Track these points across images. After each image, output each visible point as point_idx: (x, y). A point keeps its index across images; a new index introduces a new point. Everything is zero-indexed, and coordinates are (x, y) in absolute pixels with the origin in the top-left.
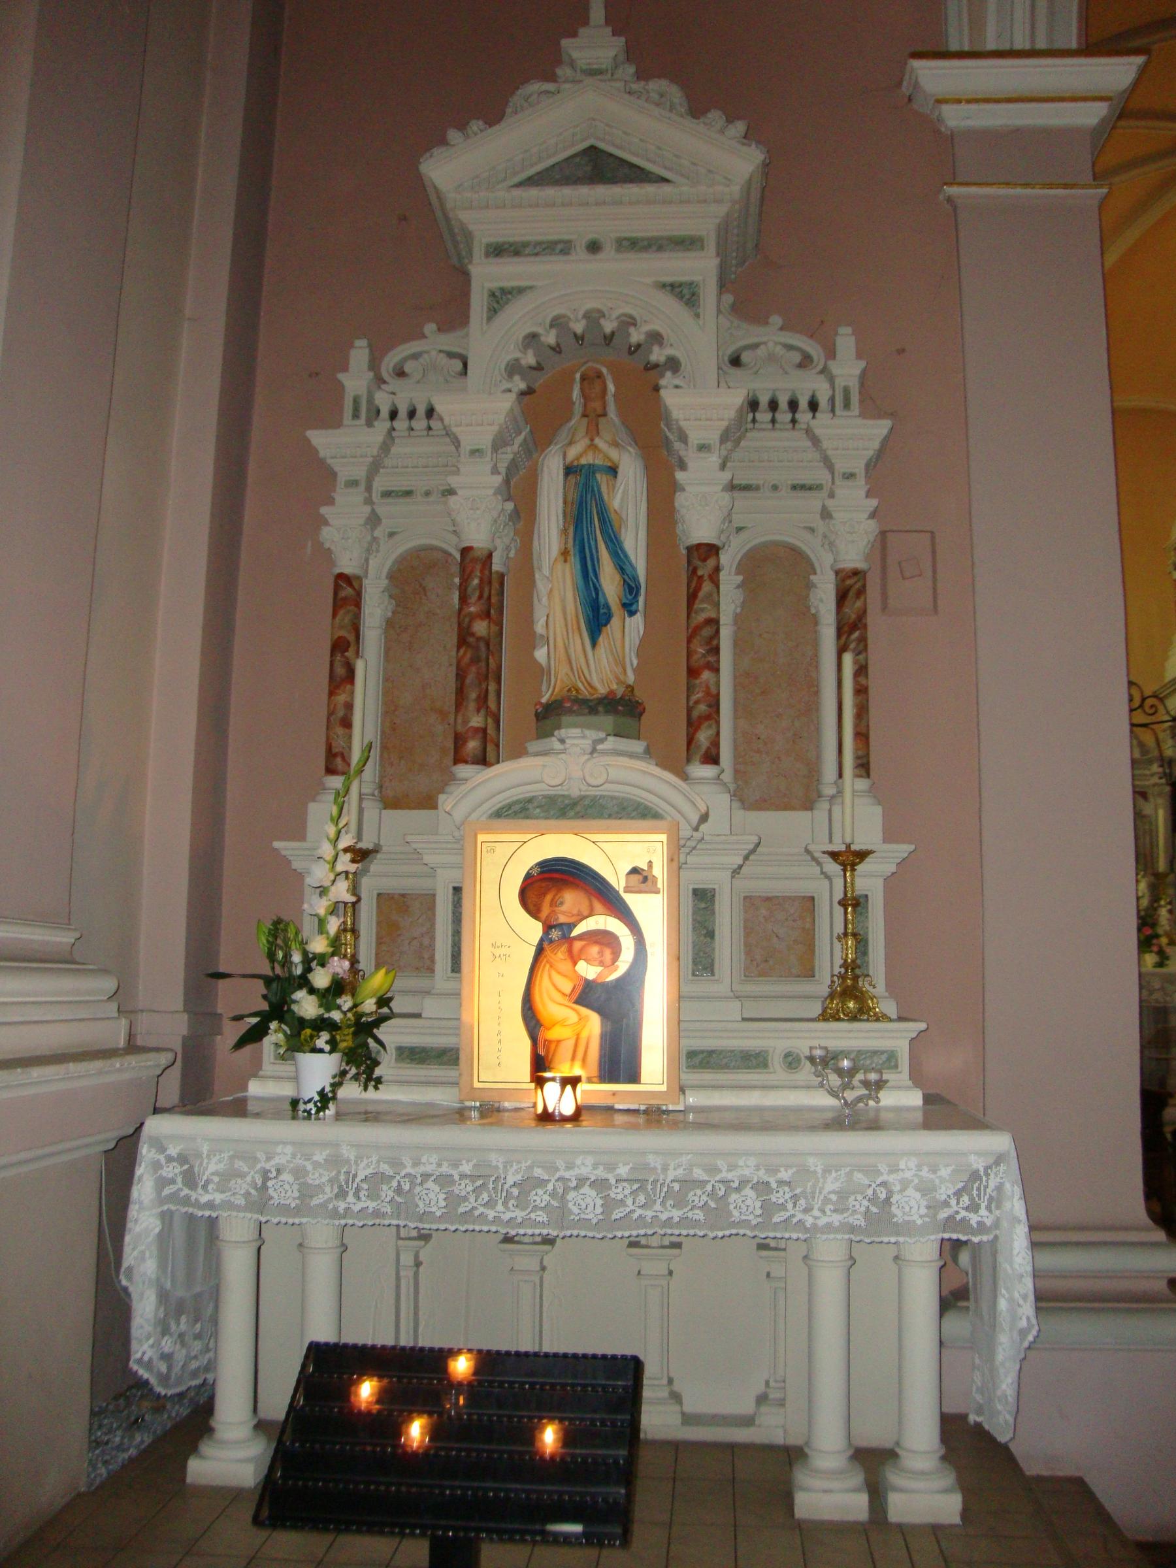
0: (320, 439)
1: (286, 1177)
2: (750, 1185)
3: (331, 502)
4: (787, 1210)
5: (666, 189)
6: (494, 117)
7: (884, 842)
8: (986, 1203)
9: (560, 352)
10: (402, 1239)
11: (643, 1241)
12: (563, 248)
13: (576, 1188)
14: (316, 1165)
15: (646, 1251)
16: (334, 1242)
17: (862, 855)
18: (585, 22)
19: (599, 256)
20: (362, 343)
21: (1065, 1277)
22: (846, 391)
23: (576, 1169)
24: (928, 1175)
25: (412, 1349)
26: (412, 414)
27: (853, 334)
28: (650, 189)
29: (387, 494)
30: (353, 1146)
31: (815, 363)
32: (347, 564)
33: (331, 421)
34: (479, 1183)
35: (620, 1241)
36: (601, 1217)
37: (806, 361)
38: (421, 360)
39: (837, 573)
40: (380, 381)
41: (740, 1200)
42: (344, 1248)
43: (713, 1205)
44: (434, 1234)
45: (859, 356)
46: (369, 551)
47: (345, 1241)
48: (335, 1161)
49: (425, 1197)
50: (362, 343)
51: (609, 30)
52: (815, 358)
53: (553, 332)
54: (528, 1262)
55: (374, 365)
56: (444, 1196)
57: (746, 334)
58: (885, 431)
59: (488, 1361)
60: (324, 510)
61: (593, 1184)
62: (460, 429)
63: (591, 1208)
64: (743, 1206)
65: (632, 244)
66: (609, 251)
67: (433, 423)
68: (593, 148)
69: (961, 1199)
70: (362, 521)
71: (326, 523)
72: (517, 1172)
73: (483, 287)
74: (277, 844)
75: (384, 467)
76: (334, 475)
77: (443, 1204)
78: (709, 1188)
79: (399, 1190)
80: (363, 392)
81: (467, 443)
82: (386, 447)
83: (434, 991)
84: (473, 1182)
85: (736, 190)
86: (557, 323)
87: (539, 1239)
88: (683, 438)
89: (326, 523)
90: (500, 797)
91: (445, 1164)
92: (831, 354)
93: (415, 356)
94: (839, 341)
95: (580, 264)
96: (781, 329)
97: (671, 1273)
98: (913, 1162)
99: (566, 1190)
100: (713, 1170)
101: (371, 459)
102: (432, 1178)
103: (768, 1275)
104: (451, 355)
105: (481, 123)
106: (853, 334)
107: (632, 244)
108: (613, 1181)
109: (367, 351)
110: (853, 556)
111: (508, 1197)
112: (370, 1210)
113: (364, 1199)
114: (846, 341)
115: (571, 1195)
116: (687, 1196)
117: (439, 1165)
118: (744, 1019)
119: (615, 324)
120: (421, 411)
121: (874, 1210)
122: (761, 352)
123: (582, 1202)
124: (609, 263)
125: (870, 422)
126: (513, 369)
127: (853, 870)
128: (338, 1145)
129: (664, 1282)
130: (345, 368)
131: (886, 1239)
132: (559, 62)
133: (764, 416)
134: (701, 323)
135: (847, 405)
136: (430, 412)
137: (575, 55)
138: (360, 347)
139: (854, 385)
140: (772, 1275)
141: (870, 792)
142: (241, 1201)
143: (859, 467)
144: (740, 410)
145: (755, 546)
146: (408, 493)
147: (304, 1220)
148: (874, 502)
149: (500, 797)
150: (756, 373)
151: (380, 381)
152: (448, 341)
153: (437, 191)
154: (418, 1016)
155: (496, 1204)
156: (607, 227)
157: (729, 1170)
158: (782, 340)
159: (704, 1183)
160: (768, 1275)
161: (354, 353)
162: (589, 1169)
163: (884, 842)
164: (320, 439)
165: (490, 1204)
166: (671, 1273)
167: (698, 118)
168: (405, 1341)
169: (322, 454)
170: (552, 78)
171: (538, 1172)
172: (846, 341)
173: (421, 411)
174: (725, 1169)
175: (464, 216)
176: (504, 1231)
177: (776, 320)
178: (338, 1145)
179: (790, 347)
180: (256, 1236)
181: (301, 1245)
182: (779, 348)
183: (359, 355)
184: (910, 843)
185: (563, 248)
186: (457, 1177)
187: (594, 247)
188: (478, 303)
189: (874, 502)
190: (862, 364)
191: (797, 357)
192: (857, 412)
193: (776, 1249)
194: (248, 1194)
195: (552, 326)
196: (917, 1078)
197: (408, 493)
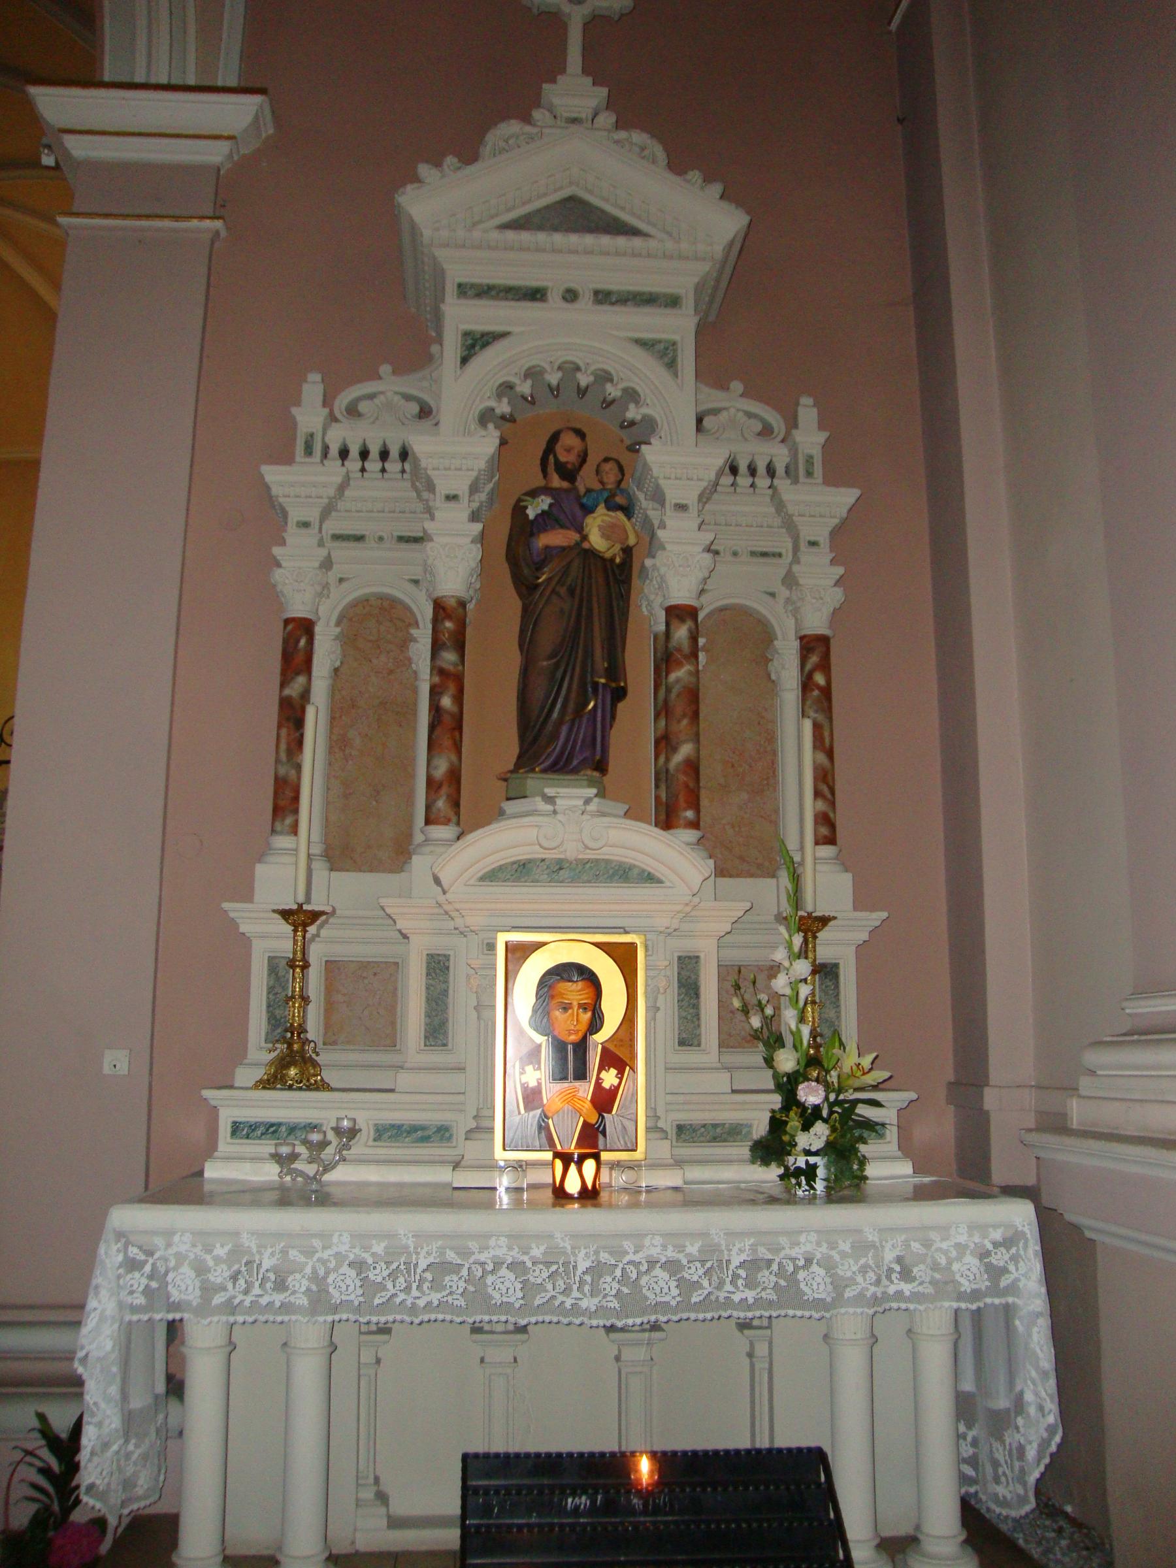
0: (273, 474)
1: (186, 1270)
2: (506, 1265)
3: (283, 543)
4: (546, 1291)
5: (637, 242)
6: (469, 156)
7: (855, 909)
8: (417, 1283)
9: (556, 397)
10: (365, 1333)
11: (487, 1327)
12: (536, 295)
13: (492, 1272)
14: (218, 1260)
15: (489, 1336)
16: (221, 1340)
17: (824, 921)
18: (563, 71)
19: (576, 305)
20: (314, 377)
21: (43, 1359)
22: (809, 460)
23: (490, 1250)
24: (674, 1254)
25: (770, 1451)
26: (364, 454)
27: (814, 405)
28: (621, 241)
29: (337, 537)
30: (253, 1234)
31: (775, 434)
32: (298, 609)
33: (285, 458)
34: (554, 1268)
35: (536, 1326)
36: (678, 1299)
37: (766, 432)
38: (376, 401)
39: (802, 638)
40: (333, 418)
41: (809, 1277)
42: (874, 1339)
43: (471, 1288)
44: (395, 1327)
45: (821, 427)
46: (320, 595)
47: (233, 1339)
48: (236, 1252)
49: (501, 1286)
50: (314, 377)
51: (589, 80)
52: (775, 425)
53: (529, 382)
54: (500, 1354)
55: (327, 401)
56: (675, 1283)
57: (713, 398)
58: (852, 500)
59: (664, 1460)
60: (277, 551)
61: (512, 1267)
62: (436, 472)
63: (511, 1291)
64: (656, 1287)
65: (603, 297)
66: (586, 301)
67: (407, 466)
68: (572, 199)
69: (1019, 1265)
70: (317, 564)
71: (279, 565)
72: (741, 1251)
73: (457, 328)
74: (226, 905)
75: (336, 511)
76: (285, 514)
77: (520, 1295)
78: (464, 1272)
79: (935, 1267)
80: (317, 428)
81: (442, 487)
82: (342, 488)
83: (407, 1065)
84: (548, 1268)
85: (718, 250)
86: (532, 374)
87: (374, 1328)
88: (658, 497)
89: (279, 565)
90: (492, 859)
91: (670, 1248)
92: (792, 422)
93: (371, 397)
94: (801, 411)
95: (552, 311)
96: (742, 395)
97: (378, 1361)
98: (658, 1240)
99: (797, 1268)
100: (465, 1253)
101: (326, 501)
102: (659, 1265)
103: (482, 1360)
104: (408, 398)
105: (455, 160)
106: (814, 405)
107: (603, 297)
108: (684, 1262)
109: (321, 387)
110: (816, 623)
111: (735, 1277)
112: (278, 1304)
113: (896, 1281)
114: (808, 413)
115: (644, 1280)
116: (444, 1281)
117: (664, 1247)
118: (734, 1091)
119: (591, 379)
120: (394, 452)
121: (625, 1290)
122: (724, 416)
123: (501, 1286)
124: (585, 312)
125: (833, 489)
126: (485, 417)
127: (815, 937)
128: (237, 1234)
129: (509, 1371)
130: (298, 403)
131: (791, 1312)
132: (537, 103)
133: (744, 481)
134: (679, 381)
135: (809, 474)
136: (404, 455)
137: (556, 101)
138: (314, 382)
139: (817, 452)
140: (486, 1360)
141: (837, 858)
142: (303, 1301)
143: (823, 536)
144: (720, 474)
145: (746, 606)
146: (359, 538)
147: (294, 1318)
148: (840, 570)
149: (492, 859)
150: (717, 439)
151: (333, 418)
152: (411, 384)
153: (414, 227)
154: (392, 1091)
155: (571, 1290)
156: (588, 279)
157: (636, 1252)
158: (746, 408)
159: (769, 1263)
160: (482, 1360)
161: (306, 388)
162: (658, 1250)
163: (855, 909)
164: (273, 474)
165: (567, 1291)
166: (378, 1361)
167: (680, 175)
168: (763, 1443)
169: (275, 491)
170: (527, 119)
171: (451, 1256)
172: (808, 413)
173: (394, 452)
174: (787, 1246)
175: (441, 254)
176: (471, 1320)
177: (737, 386)
178: (237, 1234)
179: (750, 415)
180: (952, 1330)
181: (285, 1344)
182: (740, 414)
183: (313, 388)
184: (882, 910)
185: (536, 295)
186: (529, 1264)
187: (571, 296)
188: (451, 347)
189: (840, 570)
190: (825, 435)
191: (759, 427)
192: (820, 480)
193: (492, 1332)
194: (308, 1290)
195: (559, 368)
196: (906, 1148)
197: (359, 538)
